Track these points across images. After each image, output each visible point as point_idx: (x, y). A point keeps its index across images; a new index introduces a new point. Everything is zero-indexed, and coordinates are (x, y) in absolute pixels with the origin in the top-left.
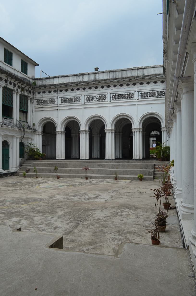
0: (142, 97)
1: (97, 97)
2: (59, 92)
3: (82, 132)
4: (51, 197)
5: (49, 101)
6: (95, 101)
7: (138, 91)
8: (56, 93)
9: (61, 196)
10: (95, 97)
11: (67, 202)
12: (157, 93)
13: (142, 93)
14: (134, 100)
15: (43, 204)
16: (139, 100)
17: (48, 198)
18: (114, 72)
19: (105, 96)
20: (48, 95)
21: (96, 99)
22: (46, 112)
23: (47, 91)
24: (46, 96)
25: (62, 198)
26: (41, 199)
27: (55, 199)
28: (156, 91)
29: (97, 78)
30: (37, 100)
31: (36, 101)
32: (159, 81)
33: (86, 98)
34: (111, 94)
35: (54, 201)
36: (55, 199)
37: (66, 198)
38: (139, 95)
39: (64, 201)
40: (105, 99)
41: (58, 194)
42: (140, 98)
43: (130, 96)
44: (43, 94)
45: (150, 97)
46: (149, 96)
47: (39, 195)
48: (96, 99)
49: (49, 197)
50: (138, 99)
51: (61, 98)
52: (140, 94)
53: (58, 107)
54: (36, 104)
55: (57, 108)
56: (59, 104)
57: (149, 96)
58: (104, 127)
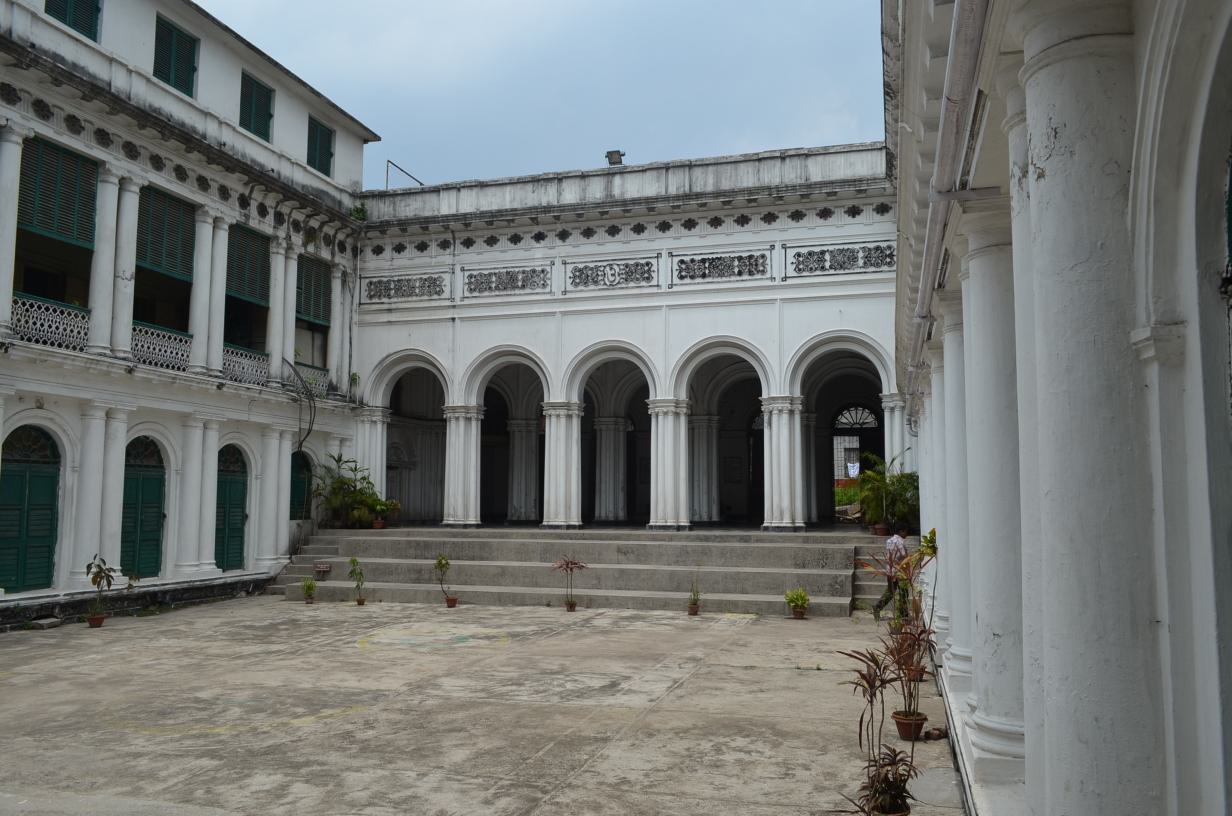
0: (800, 270)
1: (615, 267)
2: (460, 248)
3: (553, 412)
4: (417, 687)
5: (417, 285)
6: (608, 283)
7: (784, 247)
8: (448, 251)
9: (463, 682)
10: (608, 268)
11: (487, 709)
12: (861, 254)
13: (799, 255)
14: (769, 283)
15: (384, 715)
16: (789, 282)
17: (405, 688)
18: (664, 171)
19: (647, 264)
20: (417, 261)
21: (612, 279)
22: (395, 330)
23: (410, 242)
24: (410, 264)
25: (465, 688)
26: (377, 696)
27: (435, 692)
28: (857, 247)
29: (617, 192)
30: (368, 280)
31: (365, 282)
32: (552, 230)
33: (570, 274)
34: (363, 280)
35: (430, 702)
36: (435, 692)
37: (482, 690)
38: (789, 262)
39: (472, 704)
40: (648, 278)
41: (449, 674)
42: (791, 272)
43: (752, 265)
44: (396, 255)
45: (832, 272)
46: (827, 265)
47: (368, 677)
48: (613, 275)
49: (410, 684)
50: (785, 278)
51: (467, 274)
52: (791, 259)
53: (454, 307)
54: (364, 294)
55: (450, 314)
56: (458, 294)
57: (831, 267)
58: (644, 390)
